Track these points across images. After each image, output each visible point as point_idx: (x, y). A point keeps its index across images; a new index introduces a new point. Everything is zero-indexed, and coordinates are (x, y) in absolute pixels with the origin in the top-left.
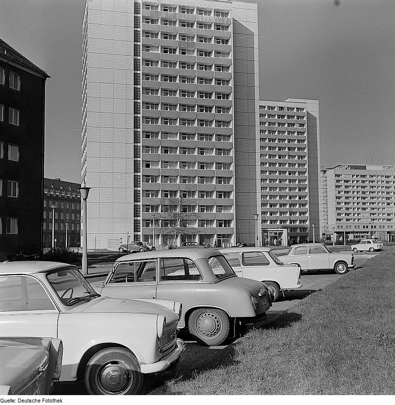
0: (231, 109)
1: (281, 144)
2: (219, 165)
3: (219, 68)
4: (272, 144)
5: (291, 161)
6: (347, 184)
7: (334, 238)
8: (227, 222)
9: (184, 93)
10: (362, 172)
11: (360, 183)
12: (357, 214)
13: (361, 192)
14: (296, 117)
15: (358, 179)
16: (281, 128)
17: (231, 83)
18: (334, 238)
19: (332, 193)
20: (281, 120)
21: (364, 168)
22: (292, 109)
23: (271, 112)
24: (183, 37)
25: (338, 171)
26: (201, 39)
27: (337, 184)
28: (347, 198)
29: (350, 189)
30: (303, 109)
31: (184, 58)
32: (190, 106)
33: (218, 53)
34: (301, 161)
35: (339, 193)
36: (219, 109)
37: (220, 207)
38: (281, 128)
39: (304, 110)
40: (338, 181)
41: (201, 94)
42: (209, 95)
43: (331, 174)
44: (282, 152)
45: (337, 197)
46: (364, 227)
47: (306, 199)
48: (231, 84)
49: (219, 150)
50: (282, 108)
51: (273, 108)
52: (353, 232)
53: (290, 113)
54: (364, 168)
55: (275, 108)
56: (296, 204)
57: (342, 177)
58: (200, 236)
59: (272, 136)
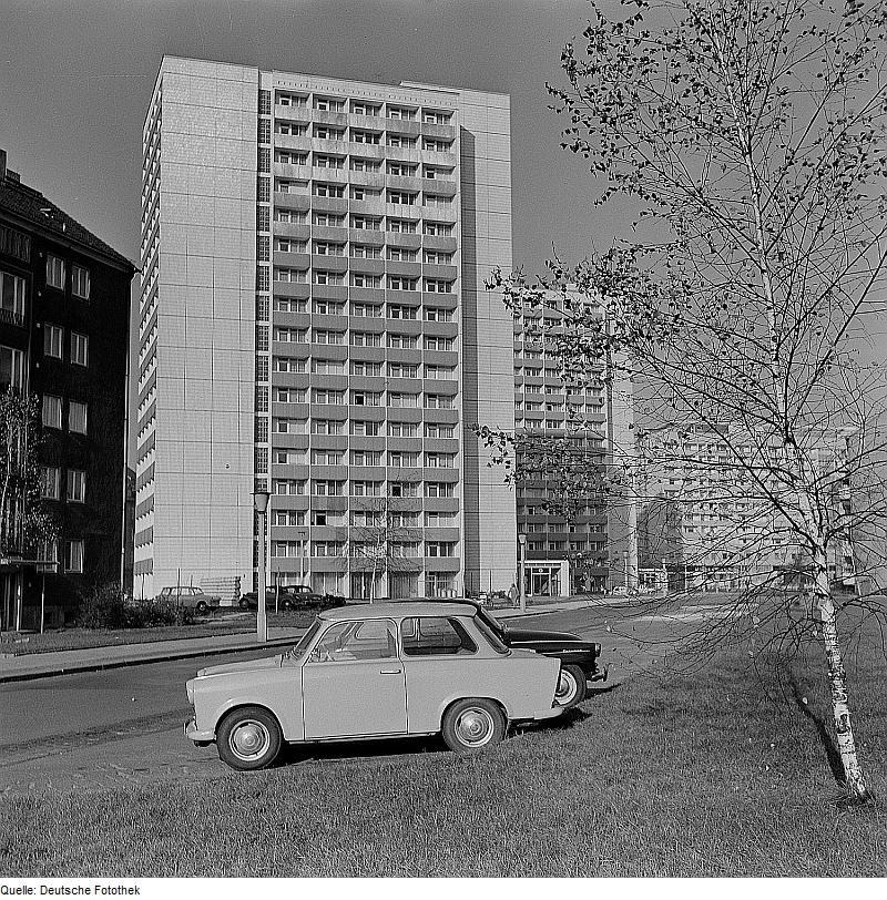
42: (410, 281)
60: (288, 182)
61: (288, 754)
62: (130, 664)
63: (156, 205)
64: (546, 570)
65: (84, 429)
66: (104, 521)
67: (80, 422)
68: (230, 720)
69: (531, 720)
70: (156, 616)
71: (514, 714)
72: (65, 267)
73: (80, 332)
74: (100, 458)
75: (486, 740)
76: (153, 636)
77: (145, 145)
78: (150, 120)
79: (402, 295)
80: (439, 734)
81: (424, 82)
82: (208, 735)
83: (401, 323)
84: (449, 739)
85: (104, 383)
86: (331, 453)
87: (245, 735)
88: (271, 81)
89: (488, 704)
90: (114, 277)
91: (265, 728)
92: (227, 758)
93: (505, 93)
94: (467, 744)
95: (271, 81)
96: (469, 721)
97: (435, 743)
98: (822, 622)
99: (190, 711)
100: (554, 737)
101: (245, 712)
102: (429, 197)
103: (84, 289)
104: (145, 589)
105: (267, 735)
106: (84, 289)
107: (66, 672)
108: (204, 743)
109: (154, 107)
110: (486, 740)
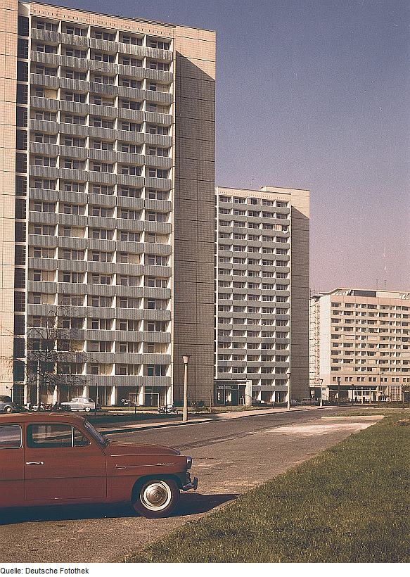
0: (170, 215)
1: (253, 255)
2: (150, 280)
3: (153, 128)
4: (239, 254)
5: (267, 280)
6: (348, 317)
7: (325, 395)
8: (161, 369)
9: (96, 165)
10: (370, 301)
11: (367, 317)
12: (361, 361)
13: (368, 314)
14: (275, 215)
15: (364, 310)
16: (253, 231)
17: (170, 218)
18: (325, 395)
19: (326, 329)
20: (253, 219)
21: (374, 294)
22: (270, 202)
23: (239, 206)
24: (96, 75)
25: (337, 298)
26: (125, 80)
27: (335, 317)
28: (348, 321)
29: (352, 356)
30: (287, 203)
31: (99, 110)
32: (105, 209)
33: (150, 234)
34: (281, 281)
35: (337, 329)
36: (152, 192)
37: (150, 346)
38: (253, 231)
39: (288, 205)
40: (335, 345)
41: (124, 168)
42: (136, 170)
43: (325, 302)
44: (253, 267)
45: (333, 368)
46: (370, 379)
47: (288, 313)
48: (171, 198)
49: (150, 257)
50: (254, 201)
51: (241, 200)
52: (353, 387)
53: (267, 208)
54: (374, 294)
55: (245, 199)
56: (272, 344)
57: (343, 308)
58: (119, 389)
59: (239, 242)
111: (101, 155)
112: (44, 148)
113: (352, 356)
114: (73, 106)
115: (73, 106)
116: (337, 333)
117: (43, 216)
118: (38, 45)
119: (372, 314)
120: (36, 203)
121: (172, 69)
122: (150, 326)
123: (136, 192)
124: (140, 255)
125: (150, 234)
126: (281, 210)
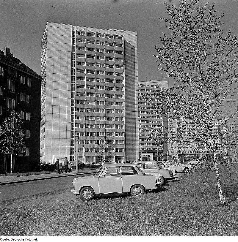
25: (180, 120)
26: (107, 51)
29: (185, 130)
33: (116, 58)
42: (111, 81)
60: (79, 55)
61: (96, 197)
62: (47, 178)
63: (45, 61)
64: (147, 155)
65: (29, 119)
66: (34, 143)
67: (28, 117)
68: (83, 189)
69: (150, 190)
70: (50, 167)
71: (147, 188)
72: (25, 78)
73: (23, 93)
74: (34, 126)
75: (141, 194)
76: (49, 172)
77: (42, 45)
78: (43, 38)
79: (109, 84)
80: (129, 193)
81: (115, 29)
82: (78, 193)
83: (90, 75)
84: (132, 193)
85: (35, 109)
86: (91, 125)
87: (85, 193)
88: (75, 29)
89: (141, 186)
90: (37, 80)
91: (90, 191)
92: (84, 199)
93: (136, 31)
94: (136, 195)
95: (75, 29)
96: (136, 190)
97: (129, 195)
98: (215, 167)
99: (73, 188)
100: (155, 194)
101: (86, 187)
102: (116, 58)
103: (30, 84)
104: (45, 159)
105: (91, 192)
106: (30, 84)
107: (32, 180)
108: (76, 195)
109: (44, 35)
110: (141, 194)
111: (100, 76)
112: (80, 74)
113: (185, 130)
114: (90, 60)
115: (90, 60)
116: (179, 127)
117: (80, 97)
118: (78, 40)
119: (193, 126)
120: (78, 70)
121: (123, 46)
122: (117, 81)
123: (111, 66)
124: (113, 110)
125: (116, 58)
126: (158, 89)
